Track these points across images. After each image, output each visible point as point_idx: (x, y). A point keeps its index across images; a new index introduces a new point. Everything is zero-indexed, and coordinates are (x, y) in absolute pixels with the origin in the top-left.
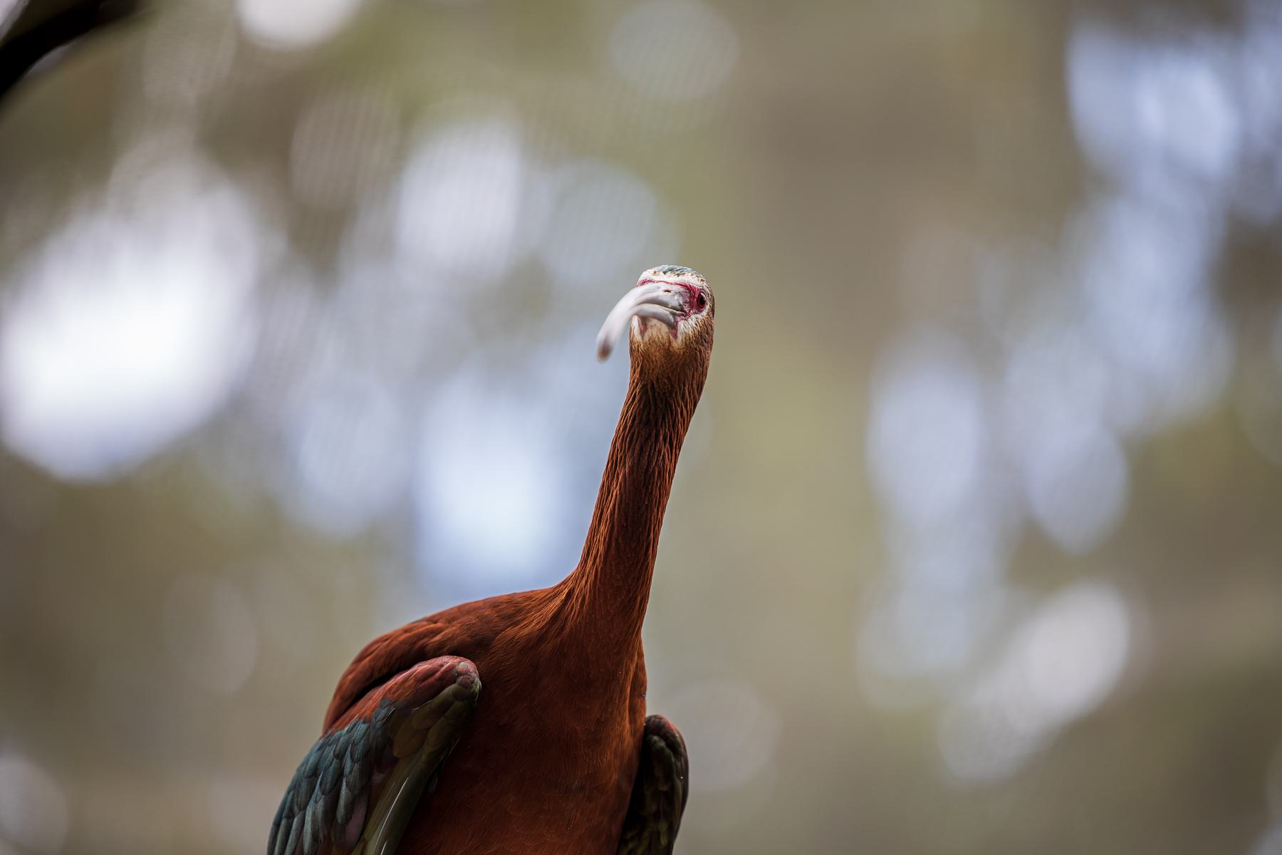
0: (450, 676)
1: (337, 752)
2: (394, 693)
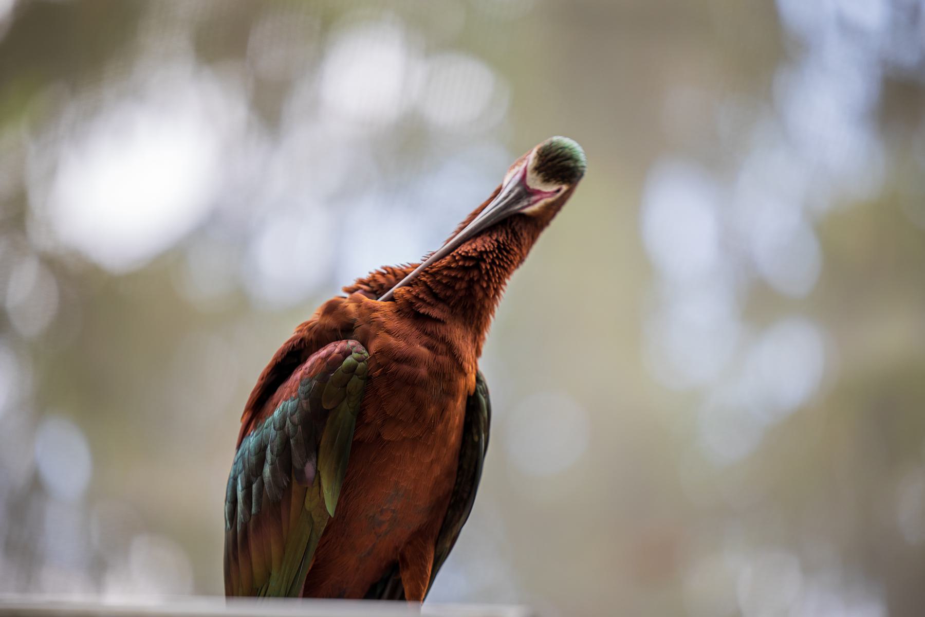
0: (346, 353)
1: (277, 426)
2: (309, 373)
